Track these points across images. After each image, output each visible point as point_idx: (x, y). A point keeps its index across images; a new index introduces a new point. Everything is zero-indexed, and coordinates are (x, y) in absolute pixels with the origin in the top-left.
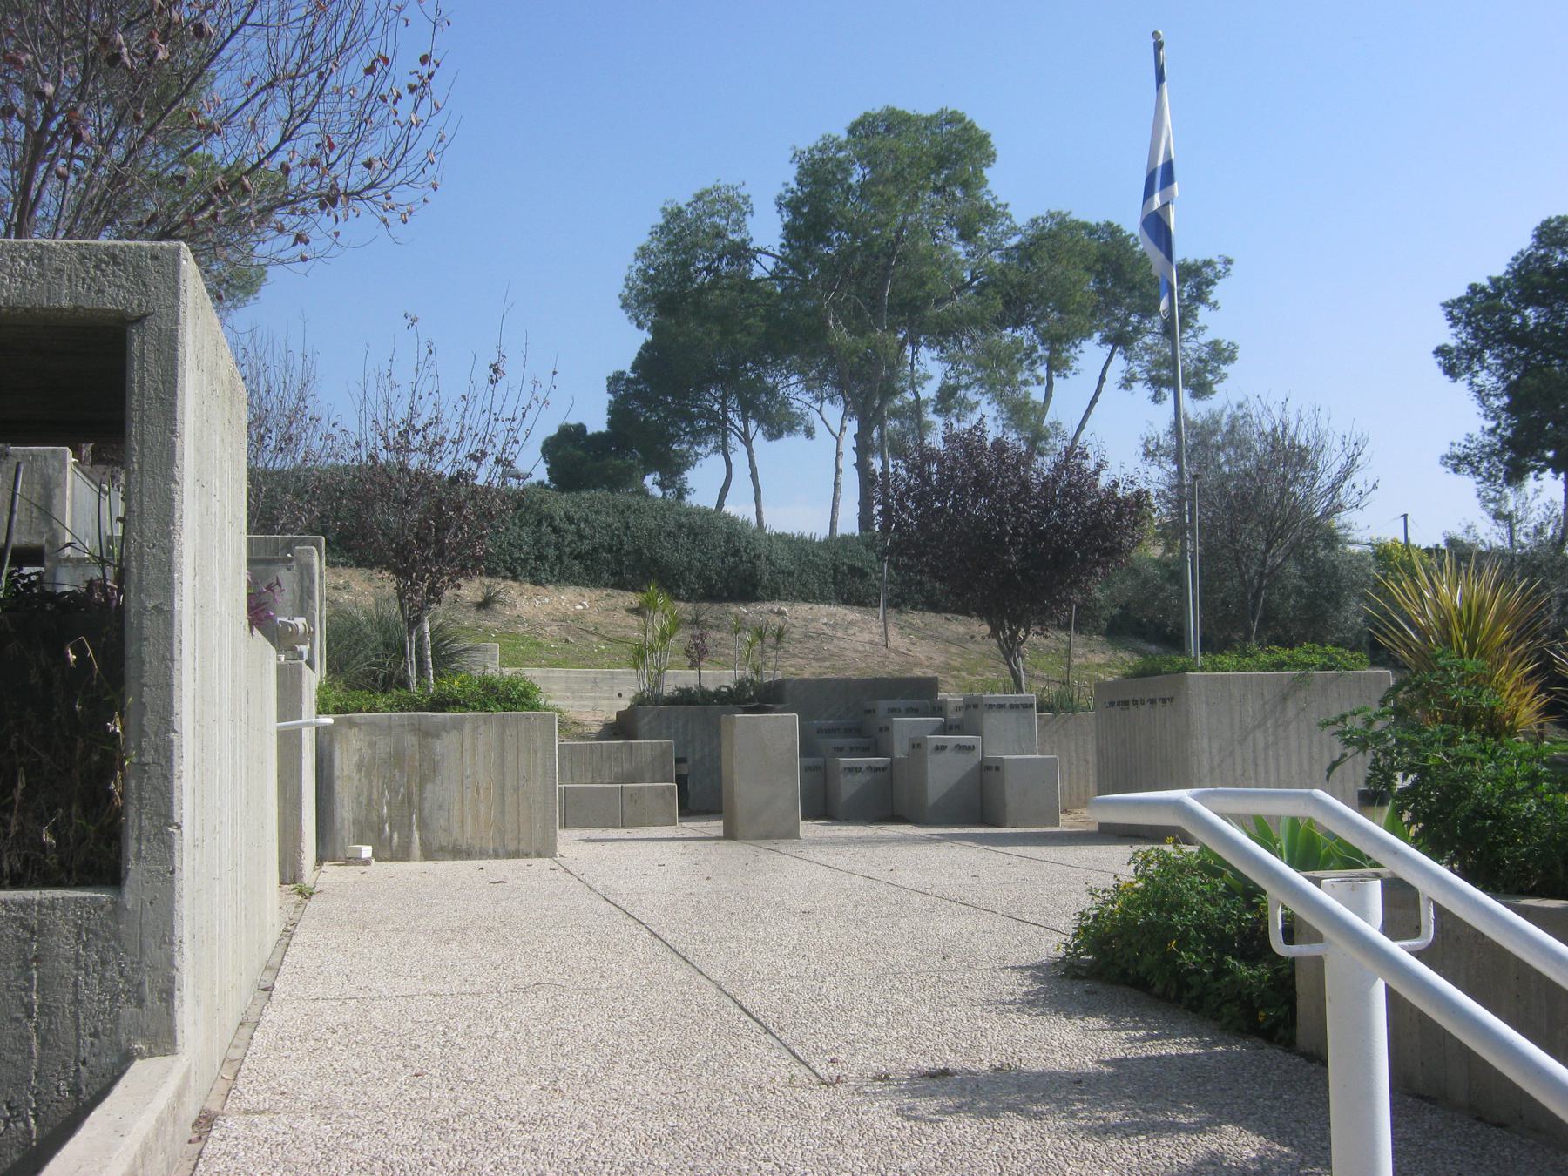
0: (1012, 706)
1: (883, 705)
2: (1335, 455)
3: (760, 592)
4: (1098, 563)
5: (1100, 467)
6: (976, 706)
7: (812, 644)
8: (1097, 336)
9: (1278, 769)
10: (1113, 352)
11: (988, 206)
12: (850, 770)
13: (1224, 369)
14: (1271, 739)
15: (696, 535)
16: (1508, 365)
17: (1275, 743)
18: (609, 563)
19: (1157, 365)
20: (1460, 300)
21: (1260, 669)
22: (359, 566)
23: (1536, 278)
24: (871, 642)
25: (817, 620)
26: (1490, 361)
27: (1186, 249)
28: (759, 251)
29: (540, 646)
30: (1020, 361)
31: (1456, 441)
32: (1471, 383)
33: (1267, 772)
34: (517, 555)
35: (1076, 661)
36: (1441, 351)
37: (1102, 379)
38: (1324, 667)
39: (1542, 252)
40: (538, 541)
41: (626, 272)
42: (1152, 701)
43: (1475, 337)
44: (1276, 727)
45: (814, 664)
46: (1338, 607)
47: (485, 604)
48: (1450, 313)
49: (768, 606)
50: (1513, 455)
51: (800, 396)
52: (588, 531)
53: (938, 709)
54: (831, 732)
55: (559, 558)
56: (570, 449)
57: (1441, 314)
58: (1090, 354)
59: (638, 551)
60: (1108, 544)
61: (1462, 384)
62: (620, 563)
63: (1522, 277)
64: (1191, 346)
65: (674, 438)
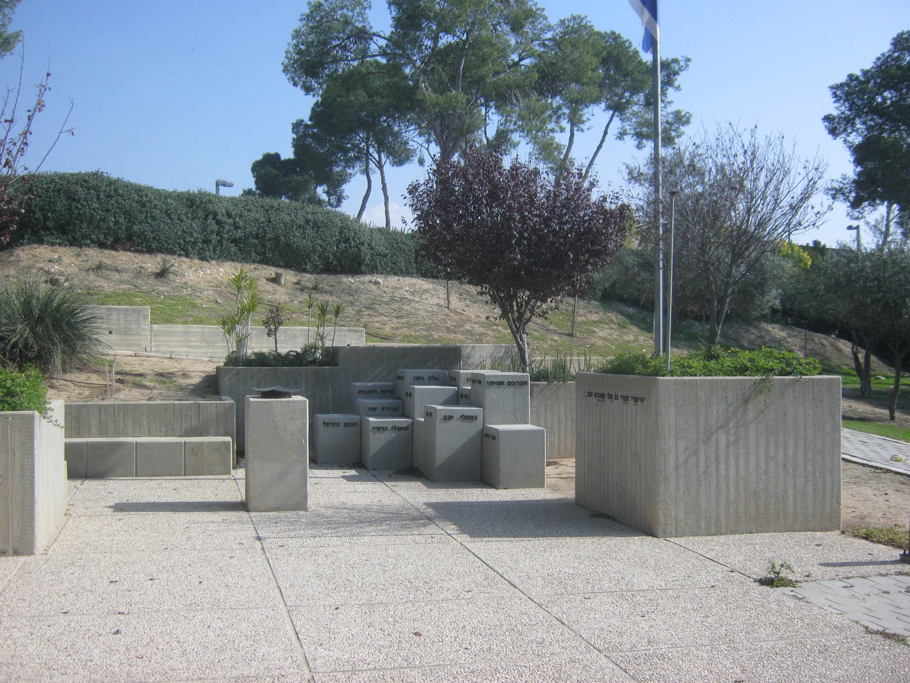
0: (509, 383)
1: (410, 373)
2: (799, 178)
3: (363, 268)
4: (587, 262)
5: (592, 185)
6: (480, 382)
7: (395, 306)
8: (603, 105)
9: (737, 467)
10: (613, 116)
11: (531, 10)
12: (378, 429)
13: (683, 129)
14: (732, 439)
15: (318, 227)
16: (870, 129)
17: (736, 442)
18: (256, 246)
19: (640, 125)
20: (842, 85)
21: (725, 374)
22: (71, 245)
23: (888, 73)
24: (438, 305)
25: (401, 288)
26: (858, 126)
27: (664, 54)
28: (374, 34)
29: (194, 306)
30: (550, 117)
31: (835, 178)
32: (845, 141)
33: (727, 469)
34: (188, 239)
35: (579, 319)
36: (828, 118)
37: (606, 133)
38: (783, 373)
39: (896, 54)
40: (204, 230)
41: (286, 48)
42: (626, 398)
43: (850, 110)
44: (738, 427)
45: (395, 321)
46: (763, 293)
47: (162, 274)
48: (835, 93)
49: (367, 278)
50: (863, 191)
51: (415, 139)
52: (241, 224)
53: (452, 380)
54: (369, 393)
55: (220, 242)
56: (269, 169)
57: (829, 94)
58: (597, 115)
59: (277, 239)
60: (596, 247)
61: (839, 141)
62: (264, 246)
63: (883, 71)
64: (664, 113)
65: (336, 163)
